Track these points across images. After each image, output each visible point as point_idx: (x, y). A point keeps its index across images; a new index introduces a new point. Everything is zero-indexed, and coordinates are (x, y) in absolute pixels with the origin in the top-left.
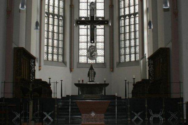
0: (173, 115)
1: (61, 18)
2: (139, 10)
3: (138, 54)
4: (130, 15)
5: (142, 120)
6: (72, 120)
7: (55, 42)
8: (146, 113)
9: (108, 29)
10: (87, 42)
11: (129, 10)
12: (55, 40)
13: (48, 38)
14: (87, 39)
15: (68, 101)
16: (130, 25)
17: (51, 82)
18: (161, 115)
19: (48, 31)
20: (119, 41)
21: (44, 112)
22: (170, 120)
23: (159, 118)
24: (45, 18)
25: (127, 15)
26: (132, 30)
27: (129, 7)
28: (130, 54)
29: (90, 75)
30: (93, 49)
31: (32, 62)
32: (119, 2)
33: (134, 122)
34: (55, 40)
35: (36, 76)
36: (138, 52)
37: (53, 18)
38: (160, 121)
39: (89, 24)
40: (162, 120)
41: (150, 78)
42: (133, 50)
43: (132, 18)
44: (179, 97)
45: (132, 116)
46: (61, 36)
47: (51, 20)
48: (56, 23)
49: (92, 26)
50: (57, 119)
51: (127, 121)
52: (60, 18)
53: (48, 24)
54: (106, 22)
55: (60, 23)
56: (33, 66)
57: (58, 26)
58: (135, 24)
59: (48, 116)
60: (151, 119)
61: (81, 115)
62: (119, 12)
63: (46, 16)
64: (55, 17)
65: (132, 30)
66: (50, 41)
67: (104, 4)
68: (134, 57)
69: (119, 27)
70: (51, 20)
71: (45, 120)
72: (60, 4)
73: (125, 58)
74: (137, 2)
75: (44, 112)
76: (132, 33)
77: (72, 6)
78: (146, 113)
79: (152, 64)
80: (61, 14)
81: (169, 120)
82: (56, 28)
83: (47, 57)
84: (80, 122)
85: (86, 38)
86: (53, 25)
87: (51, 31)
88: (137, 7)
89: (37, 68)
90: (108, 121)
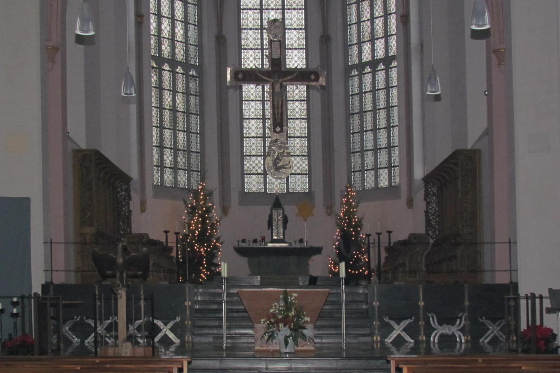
0: (493, 330)
1: (193, 72)
2: (397, 48)
3: (396, 168)
4: (374, 63)
5: (412, 341)
6: (229, 341)
7: (181, 136)
8: (422, 323)
9: (316, 96)
10: (264, 137)
11: (373, 50)
12: (179, 130)
13: (161, 127)
14: (264, 110)
15: (219, 291)
16: (374, 91)
17: (169, 241)
18: (460, 328)
19: (161, 108)
20: (348, 133)
21: (155, 321)
22: (485, 340)
23: (453, 336)
24: (150, 71)
25: (366, 64)
26: (382, 103)
27: (372, 40)
28: (376, 169)
29: (274, 223)
30: (280, 149)
31: (122, 190)
32: (345, 6)
33: (390, 346)
34: (179, 130)
35: (133, 226)
36: (397, 164)
37: (173, 72)
38: (458, 345)
39: (267, 82)
40: (463, 341)
41: (430, 232)
42: (383, 158)
43: (379, 73)
44: (506, 281)
45: (387, 329)
46: (195, 121)
47: (167, 76)
48: (180, 87)
49: (277, 87)
50: (192, 338)
51: (373, 342)
52: (191, 73)
53: (160, 88)
54: (313, 77)
55: (191, 85)
56: (125, 199)
57: (187, 94)
58: (388, 88)
59: (166, 330)
60: (434, 338)
61: (252, 327)
62: (346, 55)
63: (155, 66)
65: (382, 103)
66: (167, 134)
67: (306, 33)
68: (386, 177)
69: (347, 96)
70: (167, 76)
71: (160, 341)
72: (190, 34)
73: (363, 180)
74: (393, 8)
75: (155, 321)
76: (380, 92)
77: (220, 40)
78: (422, 323)
79: (434, 194)
80: (192, 62)
81: (483, 342)
82: (180, 99)
83: (162, 177)
84: (253, 345)
85: (260, 106)
86: (174, 92)
87: (168, 107)
88: (393, 42)
89: (135, 205)
90: (322, 343)
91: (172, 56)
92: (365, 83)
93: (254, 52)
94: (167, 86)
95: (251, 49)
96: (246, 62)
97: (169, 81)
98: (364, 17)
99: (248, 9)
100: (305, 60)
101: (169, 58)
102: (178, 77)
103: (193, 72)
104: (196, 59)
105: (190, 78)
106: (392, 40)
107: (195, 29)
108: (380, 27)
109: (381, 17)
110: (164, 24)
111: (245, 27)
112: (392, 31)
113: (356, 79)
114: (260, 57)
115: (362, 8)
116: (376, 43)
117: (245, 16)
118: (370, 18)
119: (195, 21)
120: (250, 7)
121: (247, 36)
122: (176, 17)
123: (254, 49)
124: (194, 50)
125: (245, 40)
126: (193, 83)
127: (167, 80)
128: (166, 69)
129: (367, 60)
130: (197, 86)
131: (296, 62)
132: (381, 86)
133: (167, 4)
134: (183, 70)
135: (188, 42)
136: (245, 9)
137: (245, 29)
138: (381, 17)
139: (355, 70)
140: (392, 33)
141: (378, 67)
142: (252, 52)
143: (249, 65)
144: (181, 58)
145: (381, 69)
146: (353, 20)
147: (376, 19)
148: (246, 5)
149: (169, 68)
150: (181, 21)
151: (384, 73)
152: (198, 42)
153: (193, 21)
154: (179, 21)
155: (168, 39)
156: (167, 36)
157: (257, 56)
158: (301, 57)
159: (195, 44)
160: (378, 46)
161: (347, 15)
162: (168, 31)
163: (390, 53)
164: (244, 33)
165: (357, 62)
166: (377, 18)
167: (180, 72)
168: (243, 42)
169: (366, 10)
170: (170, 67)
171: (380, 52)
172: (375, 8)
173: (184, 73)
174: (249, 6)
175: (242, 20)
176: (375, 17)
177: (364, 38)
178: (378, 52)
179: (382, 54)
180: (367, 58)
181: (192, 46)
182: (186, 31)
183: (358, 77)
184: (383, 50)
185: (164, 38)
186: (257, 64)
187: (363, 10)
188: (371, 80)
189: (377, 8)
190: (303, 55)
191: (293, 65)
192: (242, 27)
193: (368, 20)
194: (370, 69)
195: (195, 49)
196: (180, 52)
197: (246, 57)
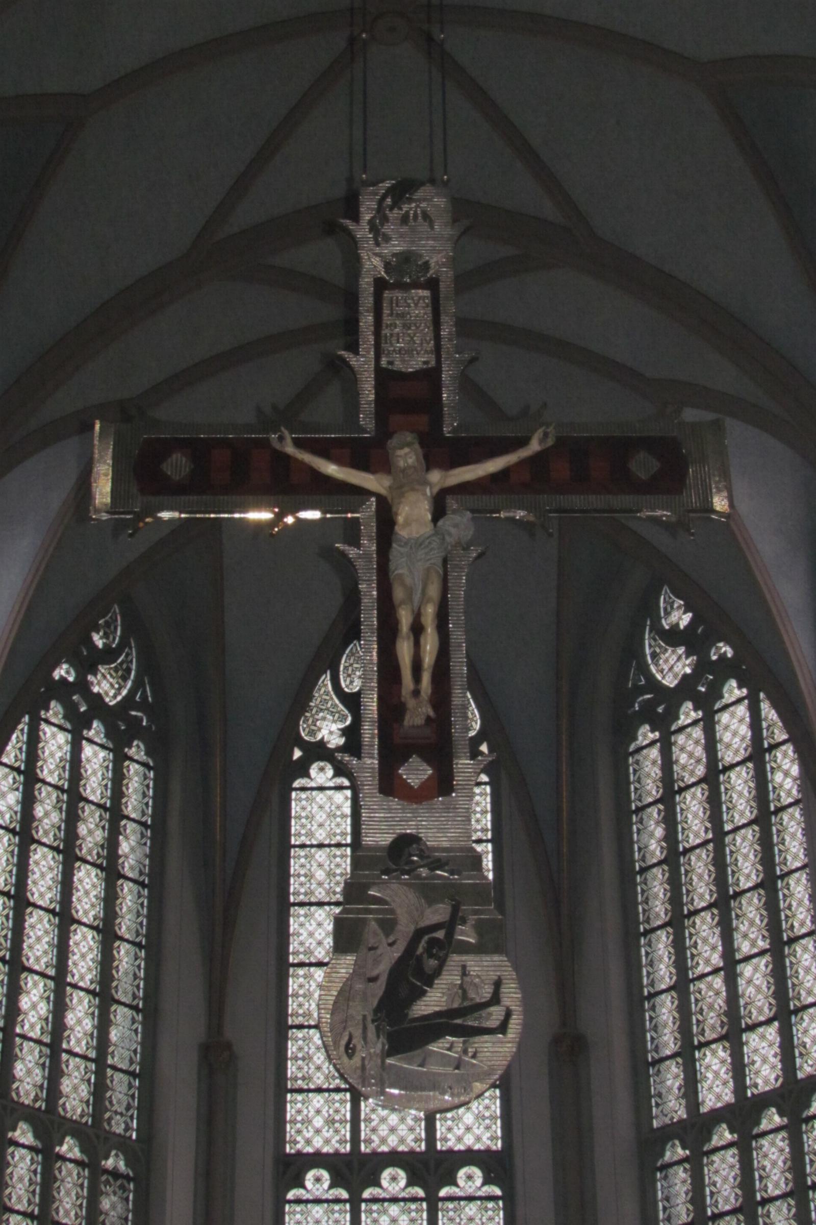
11: (739, 1068)
43: (765, 1142)
52: (110, 1163)
55: (105, 1204)
64: (132, 752)
76: (772, 1208)
91: (47, 1101)
92: (714, 1184)
93: (327, 1101)
94: (19, 1198)
95: (319, 1090)
96: (299, 1132)
97: (31, 1182)
98: (701, 962)
99: (311, 965)
100: (499, 1122)
101: (37, 1105)
102: (64, 1173)
103: (116, 1161)
104: (132, 1117)
105: (104, 1178)
106: (804, 1025)
107: (134, 1021)
108: (758, 989)
109: (762, 953)
110: (28, 993)
111: (300, 1020)
112: (803, 993)
113: (681, 1174)
114: (348, 1116)
115: (691, 935)
116: (747, 1043)
117: (300, 1049)
118: (721, 964)
119: (135, 997)
120: (320, 956)
121: (306, 1049)
122: (73, 976)
123: (328, 1090)
124: (124, 1088)
125: (300, 1062)
126: (114, 1199)
127: (21, 1179)
128: (22, 1140)
129: (719, 1105)
130: (128, 1210)
131: (468, 1129)
132: (776, 1185)
133: (46, 932)
134: (82, 1151)
135: (106, 1059)
136: (301, 965)
137: (300, 1027)
138: (762, 953)
139: (677, 1142)
140: (805, 998)
141: (758, 1123)
142: (322, 1101)
143: (308, 1142)
144: (79, 1111)
145: (771, 1127)
146: (663, 978)
147: (742, 965)
148: (305, 953)
149: (32, 1139)
150: (87, 991)
151: (783, 1140)
152: (141, 1064)
153: (130, 995)
154: (82, 989)
155: (38, 1042)
156: (36, 1033)
157: (337, 1111)
158: (487, 1114)
159: (132, 1069)
160: (756, 1051)
161: (640, 967)
162: (40, 1018)
163: (801, 1067)
164: (296, 1040)
165: (682, 1113)
166: (747, 959)
167: (70, 1155)
168: (291, 1069)
169: (705, 940)
170: (36, 1136)
171: (766, 1071)
172: (737, 929)
173: (86, 1160)
174: (316, 953)
175: (290, 1000)
176: (738, 956)
177: (703, 1033)
178: (757, 1073)
179: (773, 1077)
180: (719, 1097)
181: (121, 1075)
182: (104, 1024)
183: (687, 1166)
184: (776, 1061)
185: (24, 1037)
186: (337, 1138)
187: (696, 942)
188: (737, 1170)
189: (743, 928)
190: (493, 1107)
191: (459, 1139)
192: (290, 1022)
193: (716, 971)
194: (731, 1132)
195: (130, 1086)
196: (75, 1088)
197: (299, 1118)
